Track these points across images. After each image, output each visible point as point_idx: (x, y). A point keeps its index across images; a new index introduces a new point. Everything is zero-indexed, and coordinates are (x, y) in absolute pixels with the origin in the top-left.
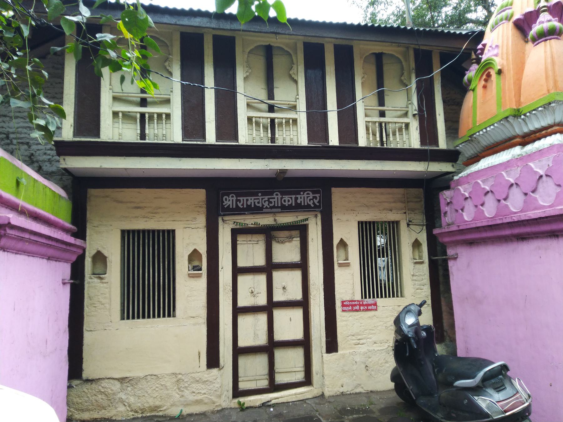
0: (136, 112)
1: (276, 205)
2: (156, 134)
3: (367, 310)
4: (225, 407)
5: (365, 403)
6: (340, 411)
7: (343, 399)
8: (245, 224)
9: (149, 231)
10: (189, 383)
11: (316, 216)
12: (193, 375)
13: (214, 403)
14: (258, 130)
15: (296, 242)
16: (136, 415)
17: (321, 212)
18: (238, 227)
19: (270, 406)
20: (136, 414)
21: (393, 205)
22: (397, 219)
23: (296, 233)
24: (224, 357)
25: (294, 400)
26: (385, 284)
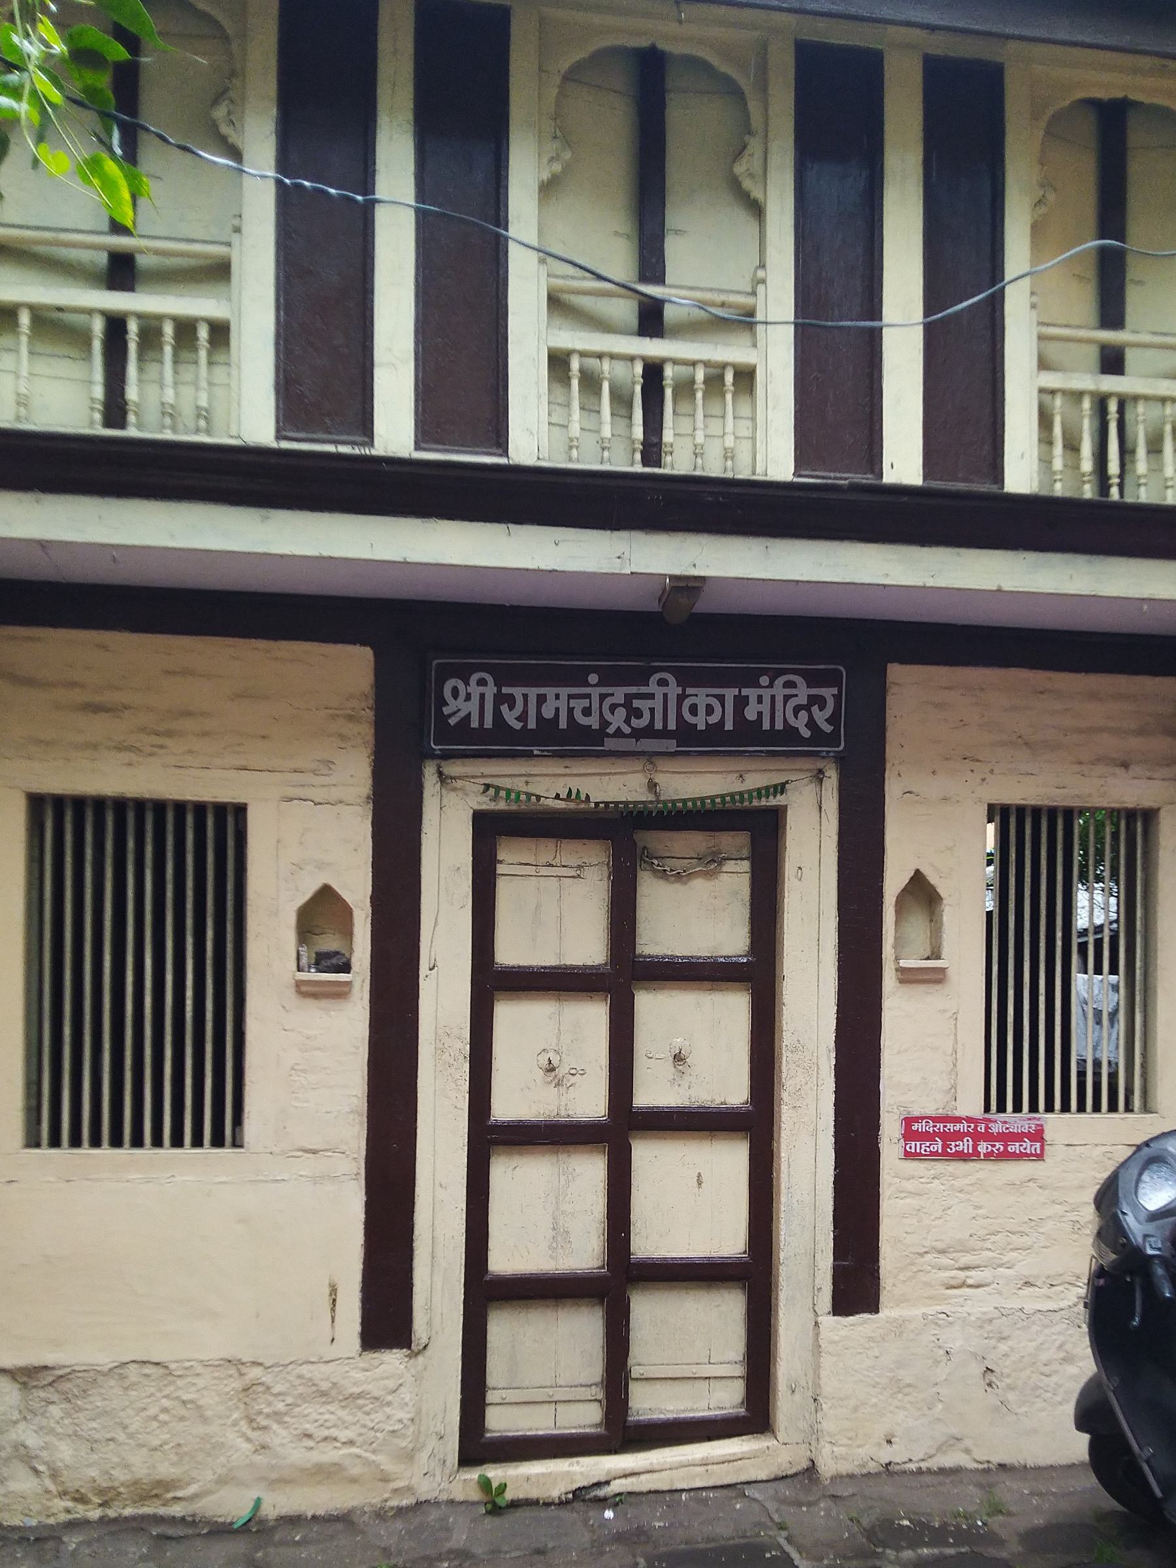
0: (90, 312)
1: (658, 725)
2: (168, 405)
3: (1006, 1156)
4: (430, 1496)
5: (971, 1509)
6: (870, 1534)
7: (888, 1489)
8: (529, 795)
9: (140, 805)
10: (289, 1400)
11: (819, 777)
12: (305, 1370)
13: (385, 1479)
14: (590, 410)
15: (736, 880)
16: (81, 1511)
17: (841, 761)
18: (502, 806)
19: (603, 1502)
20: (80, 1507)
21: (1134, 742)
22: (1147, 803)
23: (736, 841)
24: (429, 1309)
25: (699, 1484)
26: (1113, 1077)
